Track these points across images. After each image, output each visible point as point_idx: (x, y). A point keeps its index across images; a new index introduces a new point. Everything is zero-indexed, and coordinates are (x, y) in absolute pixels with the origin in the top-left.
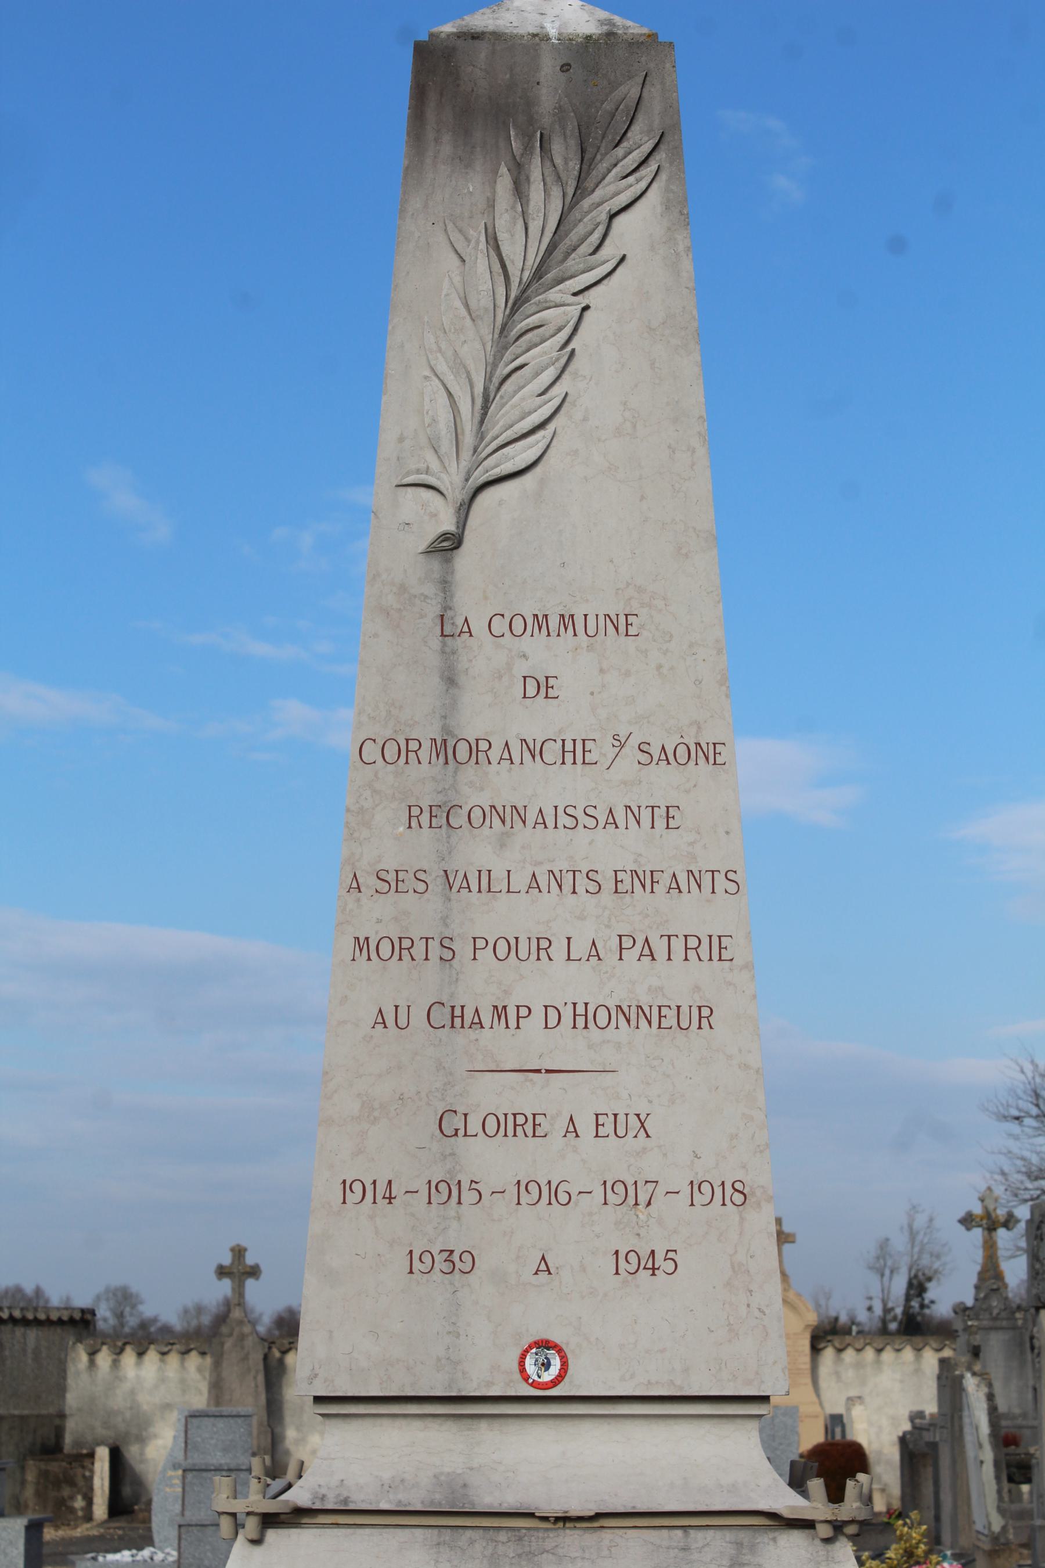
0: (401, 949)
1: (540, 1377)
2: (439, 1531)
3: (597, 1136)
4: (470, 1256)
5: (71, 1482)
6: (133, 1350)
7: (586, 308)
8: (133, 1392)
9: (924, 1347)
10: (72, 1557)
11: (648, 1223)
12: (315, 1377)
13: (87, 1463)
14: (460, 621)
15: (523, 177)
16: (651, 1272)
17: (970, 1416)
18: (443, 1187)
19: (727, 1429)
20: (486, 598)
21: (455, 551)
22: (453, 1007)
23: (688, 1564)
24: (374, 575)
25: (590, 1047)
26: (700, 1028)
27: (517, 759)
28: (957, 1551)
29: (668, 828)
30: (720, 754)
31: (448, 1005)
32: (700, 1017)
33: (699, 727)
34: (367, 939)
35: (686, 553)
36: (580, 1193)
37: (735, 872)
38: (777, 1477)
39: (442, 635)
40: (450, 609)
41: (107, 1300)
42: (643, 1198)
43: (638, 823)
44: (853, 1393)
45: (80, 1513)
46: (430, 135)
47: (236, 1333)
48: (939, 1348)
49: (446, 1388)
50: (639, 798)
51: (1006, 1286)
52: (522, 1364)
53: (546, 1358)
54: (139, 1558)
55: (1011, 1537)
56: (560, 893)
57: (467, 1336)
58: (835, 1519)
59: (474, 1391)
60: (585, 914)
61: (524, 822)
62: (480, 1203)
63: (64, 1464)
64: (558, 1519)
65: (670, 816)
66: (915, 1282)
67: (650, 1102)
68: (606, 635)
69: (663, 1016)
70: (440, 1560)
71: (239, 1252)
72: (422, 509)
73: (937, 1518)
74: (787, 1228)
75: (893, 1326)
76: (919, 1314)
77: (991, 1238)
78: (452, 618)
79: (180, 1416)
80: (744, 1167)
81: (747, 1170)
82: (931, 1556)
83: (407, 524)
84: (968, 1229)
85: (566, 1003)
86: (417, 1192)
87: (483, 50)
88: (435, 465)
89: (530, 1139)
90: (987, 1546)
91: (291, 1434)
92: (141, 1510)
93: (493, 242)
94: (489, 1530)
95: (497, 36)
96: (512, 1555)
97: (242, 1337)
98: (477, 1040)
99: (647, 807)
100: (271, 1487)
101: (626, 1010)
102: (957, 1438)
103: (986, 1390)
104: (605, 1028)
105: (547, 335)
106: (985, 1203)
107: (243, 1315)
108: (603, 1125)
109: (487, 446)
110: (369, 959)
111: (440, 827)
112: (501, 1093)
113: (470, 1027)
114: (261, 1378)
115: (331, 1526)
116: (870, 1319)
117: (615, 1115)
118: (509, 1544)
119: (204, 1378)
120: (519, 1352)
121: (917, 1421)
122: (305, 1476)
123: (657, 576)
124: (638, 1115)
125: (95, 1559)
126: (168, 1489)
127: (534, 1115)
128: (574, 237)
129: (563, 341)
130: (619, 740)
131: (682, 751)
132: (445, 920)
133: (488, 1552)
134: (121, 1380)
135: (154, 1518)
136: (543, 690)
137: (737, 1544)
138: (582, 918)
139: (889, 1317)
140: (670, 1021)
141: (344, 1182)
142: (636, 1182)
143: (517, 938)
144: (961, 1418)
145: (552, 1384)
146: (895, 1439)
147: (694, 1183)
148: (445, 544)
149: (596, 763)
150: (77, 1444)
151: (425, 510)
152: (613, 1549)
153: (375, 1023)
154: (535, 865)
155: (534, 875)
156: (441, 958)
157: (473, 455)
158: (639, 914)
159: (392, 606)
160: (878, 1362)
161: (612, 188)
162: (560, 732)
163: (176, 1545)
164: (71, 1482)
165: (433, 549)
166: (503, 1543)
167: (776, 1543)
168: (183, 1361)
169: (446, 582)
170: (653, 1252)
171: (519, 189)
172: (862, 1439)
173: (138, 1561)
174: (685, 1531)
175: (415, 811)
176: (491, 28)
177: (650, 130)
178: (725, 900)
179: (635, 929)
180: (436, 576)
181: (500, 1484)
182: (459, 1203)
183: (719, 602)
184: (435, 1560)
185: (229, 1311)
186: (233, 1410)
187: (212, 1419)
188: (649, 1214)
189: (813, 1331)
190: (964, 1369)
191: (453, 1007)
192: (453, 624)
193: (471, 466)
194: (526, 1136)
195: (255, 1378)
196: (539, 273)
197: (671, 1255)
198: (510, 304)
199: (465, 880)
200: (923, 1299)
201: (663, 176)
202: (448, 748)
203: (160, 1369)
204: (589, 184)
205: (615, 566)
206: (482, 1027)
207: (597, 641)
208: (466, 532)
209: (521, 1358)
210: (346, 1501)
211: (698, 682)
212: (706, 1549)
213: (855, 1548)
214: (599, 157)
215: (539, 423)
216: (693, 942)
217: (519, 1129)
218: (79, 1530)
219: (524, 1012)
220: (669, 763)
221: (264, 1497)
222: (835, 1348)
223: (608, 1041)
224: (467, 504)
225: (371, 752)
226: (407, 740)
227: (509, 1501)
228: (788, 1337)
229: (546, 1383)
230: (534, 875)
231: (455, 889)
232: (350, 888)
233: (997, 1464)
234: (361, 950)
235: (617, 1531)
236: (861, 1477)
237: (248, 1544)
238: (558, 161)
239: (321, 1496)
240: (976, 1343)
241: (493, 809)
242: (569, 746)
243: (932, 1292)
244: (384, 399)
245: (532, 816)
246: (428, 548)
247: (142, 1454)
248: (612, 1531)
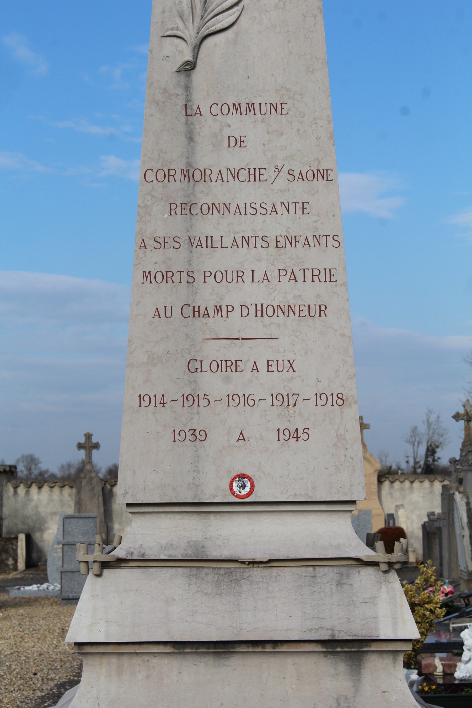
0: (167, 277)
1: (240, 492)
2: (190, 569)
3: (268, 371)
4: (204, 432)
5: (7, 552)
6: (36, 485)
8: (36, 507)
9: (434, 480)
10: (7, 588)
11: (294, 415)
12: (127, 494)
13: (14, 542)
14: (195, 107)
16: (296, 439)
17: (457, 513)
18: (190, 398)
19: (335, 517)
20: (208, 95)
21: (192, 71)
22: (194, 307)
23: (315, 584)
24: (150, 83)
25: (264, 326)
26: (320, 316)
27: (225, 179)
28: (451, 580)
29: (303, 214)
30: (330, 175)
31: (191, 306)
32: (320, 310)
33: (319, 162)
34: (150, 272)
35: (312, 71)
36: (260, 400)
37: (338, 236)
38: (360, 541)
39: (186, 115)
40: (190, 101)
41: (23, 461)
43: (288, 211)
44: (398, 503)
45: (11, 567)
47: (87, 477)
48: (442, 480)
49: (193, 498)
50: (288, 198)
52: (231, 486)
53: (243, 483)
54: (41, 588)
56: (248, 248)
57: (203, 472)
58: (389, 561)
59: (207, 500)
60: (261, 258)
61: (229, 212)
62: (209, 405)
63: (3, 543)
64: (250, 563)
65: (304, 208)
66: (430, 448)
67: (295, 354)
68: (270, 114)
69: (301, 310)
70: (191, 584)
71: (88, 436)
72: (175, 48)
73: (441, 565)
74: (365, 422)
75: (419, 471)
76: (432, 464)
77: (469, 425)
78: (191, 106)
79: (60, 518)
80: (343, 386)
81: (344, 388)
82: (438, 582)
83: (167, 57)
84: (457, 421)
85: (252, 304)
86: (177, 400)
88: (181, 25)
89: (234, 373)
90: (466, 578)
91: (116, 526)
92: (42, 565)
94: (216, 569)
96: (227, 581)
97: (91, 479)
98: (206, 323)
99: (292, 203)
100: (106, 549)
101: (282, 307)
102: (451, 524)
103: (466, 500)
104: (272, 316)
106: (466, 408)
107: (91, 468)
108: (271, 366)
109: (208, 15)
110: (151, 283)
111: (186, 214)
112: (219, 350)
113: (203, 317)
114: (101, 499)
115: (136, 567)
116: (408, 467)
117: (277, 361)
118: (225, 575)
119: (72, 499)
121: (431, 517)
122: (122, 543)
123: (297, 83)
125: (19, 589)
126: (55, 555)
127: (236, 361)
130: (278, 169)
131: (310, 174)
132: (189, 262)
133: (215, 579)
134: (30, 501)
135: (48, 569)
136: (238, 143)
137: (340, 574)
138: (259, 260)
139: (417, 466)
141: (140, 396)
142: (288, 394)
143: (226, 271)
144: (453, 514)
145: (246, 496)
146: (420, 526)
147: (318, 394)
148: (187, 67)
149: (266, 181)
150: (9, 532)
151: (176, 49)
152: (277, 577)
153: (155, 315)
154: (235, 234)
155: (235, 238)
156: (188, 282)
157: (201, 20)
158: (289, 258)
159: (160, 100)
160: (411, 488)
162: (247, 165)
163: (59, 582)
164: (7, 552)
165: (181, 70)
166: (222, 575)
167: (360, 573)
168: (61, 491)
169: (188, 87)
170: (297, 429)
172: (403, 526)
173: (41, 590)
174: (314, 568)
175: (173, 206)
178: (332, 250)
179: (286, 266)
180: (183, 84)
181: (221, 546)
182: (199, 406)
183: (329, 96)
184: (188, 583)
185: (84, 466)
187: (76, 519)
188: (295, 410)
189: (379, 473)
190: (455, 490)
191: (194, 307)
192: (192, 109)
193: (200, 25)
194: (232, 371)
195: (98, 499)
197: (306, 431)
199: (199, 242)
200: (434, 457)
202: (190, 174)
203: (50, 495)
205: (275, 78)
206: (209, 317)
207: (266, 117)
208: (198, 61)
209: (231, 483)
210: (143, 555)
211: (318, 138)
212: (325, 577)
213: (400, 578)
215: (235, 3)
216: (316, 272)
217: (228, 368)
218: (11, 575)
219: (230, 309)
220: (303, 180)
221: (102, 554)
222: (390, 481)
223: (273, 323)
224: (198, 46)
225: (150, 176)
226: (169, 170)
227: (225, 554)
228: (366, 476)
229: (244, 495)
230: (235, 238)
231: (194, 246)
232: (141, 246)
234: (147, 278)
235: (279, 568)
236: (402, 540)
237: (94, 577)
239: (131, 553)
240: (461, 477)
241: (213, 205)
242: (252, 172)
243: (439, 453)
245: (233, 208)
246: (178, 69)
247: (42, 537)
248: (277, 568)
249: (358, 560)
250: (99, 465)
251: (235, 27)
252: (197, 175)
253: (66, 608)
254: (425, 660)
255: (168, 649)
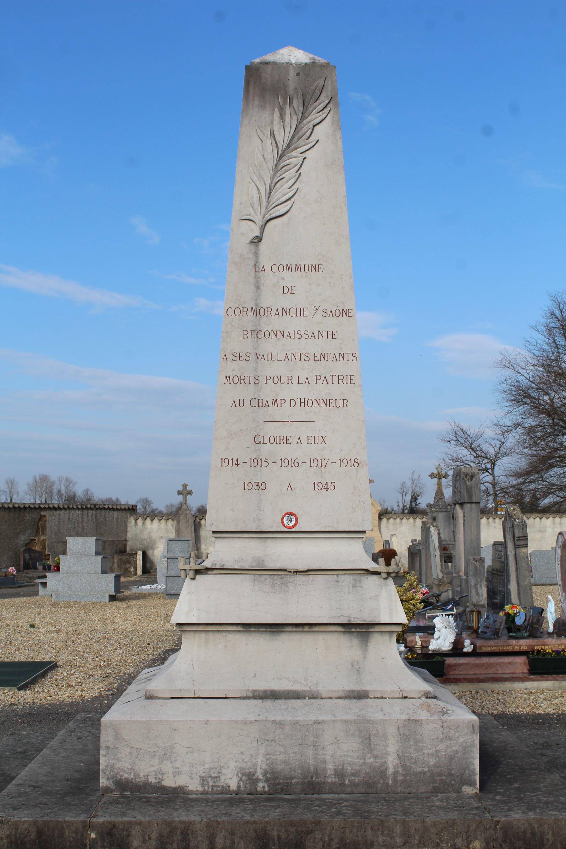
5: (129, 562)
7: (305, 158)
8: (150, 533)
15: (283, 112)
18: (255, 461)
19: (351, 542)
22: (259, 400)
26: (343, 407)
27: (281, 314)
34: (229, 376)
39: (255, 272)
41: (141, 502)
42: (323, 465)
45: (133, 573)
46: (251, 98)
51: (445, 498)
55: (445, 580)
64: (294, 572)
67: (326, 432)
71: (185, 486)
73: (421, 574)
75: (406, 511)
87: (269, 68)
88: (252, 213)
93: (273, 135)
95: (274, 63)
97: (186, 515)
102: (428, 547)
105: (292, 167)
109: (270, 206)
110: (230, 383)
114: (193, 528)
117: (314, 437)
120: (282, 516)
124: (322, 437)
125: (138, 587)
128: (301, 133)
129: (297, 170)
131: (337, 312)
140: (333, 404)
141: (222, 459)
144: (429, 541)
146: (407, 549)
148: (256, 240)
150: (131, 550)
160: (401, 523)
161: (314, 117)
162: (296, 305)
164: (129, 562)
168: (166, 523)
170: (327, 483)
171: (282, 117)
175: (246, 333)
176: (272, 60)
177: (327, 96)
180: (253, 251)
182: (261, 466)
185: (182, 506)
191: (259, 400)
195: (191, 528)
196: (289, 146)
197: (333, 484)
198: (278, 157)
201: (332, 112)
204: (306, 115)
210: (223, 566)
211: (343, 288)
212: (344, 581)
214: (309, 105)
216: (341, 378)
219: (283, 401)
225: (231, 312)
227: (278, 566)
231: (259, 359)
233: (441, 556)
237: (190, 580)
238: (295, 107)
242: (299, 310)
244: (235, 190)
245: (286, 334)
247: (153, 553)
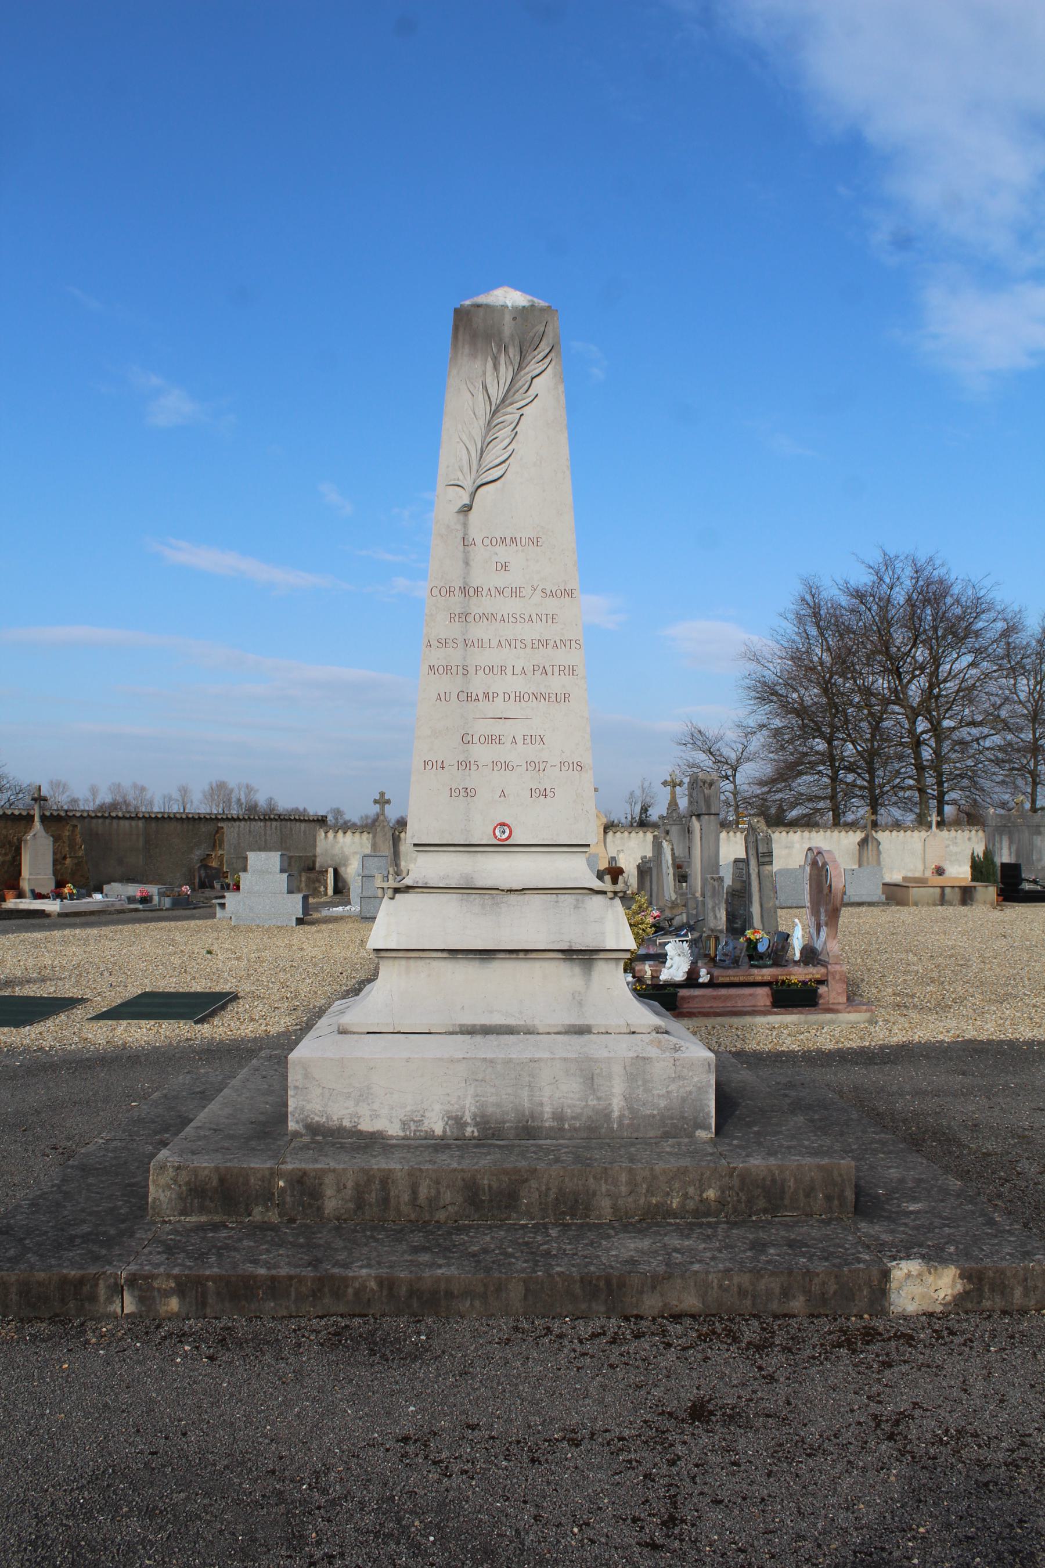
5: (319, 881)
7: (522, 415)
8: (342, 847)
13: (325, 874)
14: (471, 540)
18: (463, 763)
27: (493, 595)
42: (542, 768)
71: (382, 794)
73: (651, 896)
75: (635, 824)
87: (481, 311)
88: (461, 477)
90: (670, 905)
91: (403, 864)
97: (384, 827)
114: (391, 842)
131: (559, 592)
132: (464, 658)
140: (553, 699)
150: (321, 867)
161: (533, 367)
164: (319, 881)
171: (496, 367)
175: (453, 615)
186: (381, 854)
196: (503, 401)
201: (553, 363)
204: (524, 365)
210: (426, 883)
216: (562, 668)
219: (495, 695)
225: (435, 592)
233: (674, 875)
238: (511, 356)
242: (514, 590)
245: (499, 618)
249: (590, 889)
250: (390, 817)
251: (503, 478)
252: (472, 592)
253: (364, 925)
254: (638, 967)
255: (445, 955)
